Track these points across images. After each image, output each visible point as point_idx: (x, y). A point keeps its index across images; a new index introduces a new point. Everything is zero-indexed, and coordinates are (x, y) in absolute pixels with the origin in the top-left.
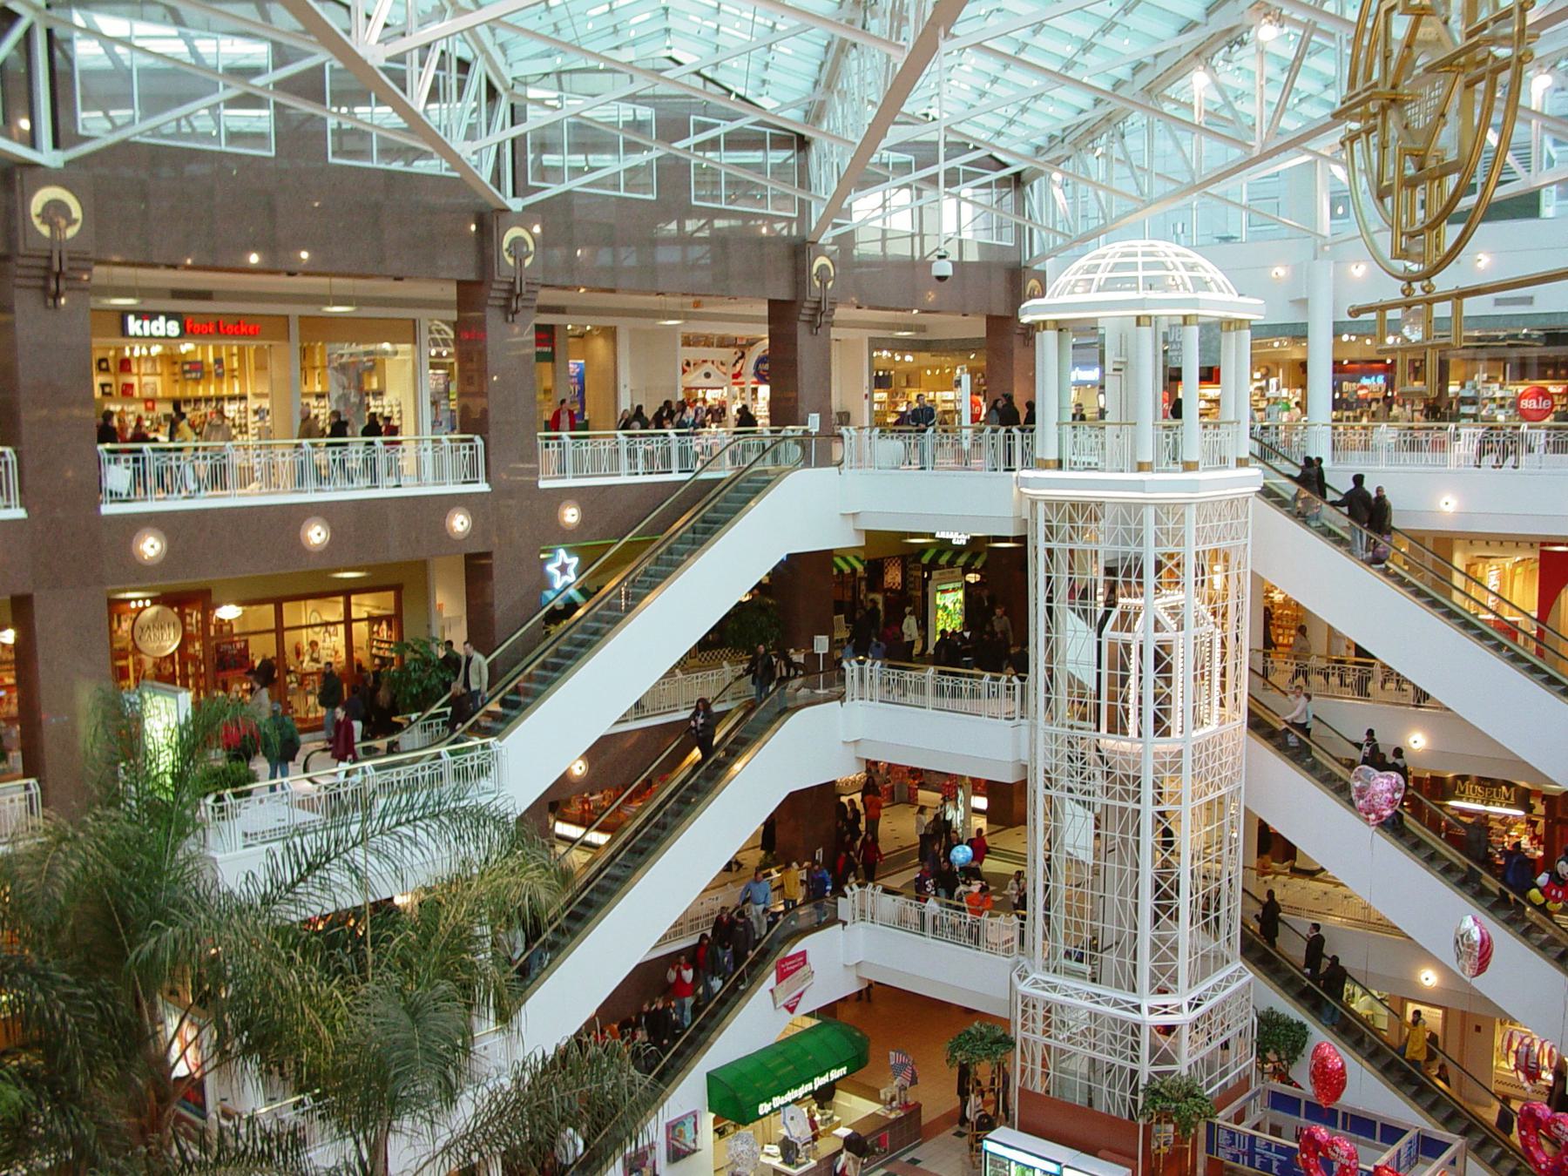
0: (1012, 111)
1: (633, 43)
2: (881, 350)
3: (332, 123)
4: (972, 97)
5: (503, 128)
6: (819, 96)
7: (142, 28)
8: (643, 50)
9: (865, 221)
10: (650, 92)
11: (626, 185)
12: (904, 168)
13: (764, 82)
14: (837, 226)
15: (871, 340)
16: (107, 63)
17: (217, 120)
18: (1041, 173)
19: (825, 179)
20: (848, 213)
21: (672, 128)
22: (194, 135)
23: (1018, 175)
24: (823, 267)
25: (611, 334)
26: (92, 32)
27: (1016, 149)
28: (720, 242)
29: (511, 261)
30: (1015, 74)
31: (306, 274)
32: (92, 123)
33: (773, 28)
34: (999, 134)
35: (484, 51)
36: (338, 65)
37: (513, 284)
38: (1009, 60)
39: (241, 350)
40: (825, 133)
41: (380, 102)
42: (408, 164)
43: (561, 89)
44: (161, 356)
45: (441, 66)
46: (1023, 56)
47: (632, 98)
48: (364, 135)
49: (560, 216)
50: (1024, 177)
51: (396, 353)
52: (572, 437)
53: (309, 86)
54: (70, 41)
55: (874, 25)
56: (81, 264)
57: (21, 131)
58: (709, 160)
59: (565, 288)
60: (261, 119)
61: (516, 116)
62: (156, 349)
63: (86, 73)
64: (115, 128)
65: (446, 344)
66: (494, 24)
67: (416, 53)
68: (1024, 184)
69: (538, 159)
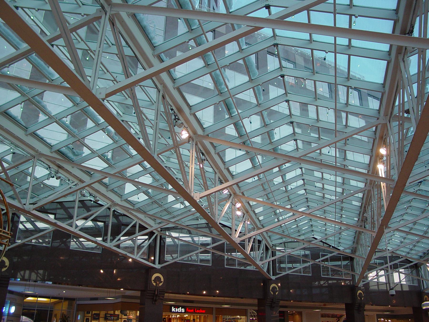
0: (411, 247)
1: (304, 234)
2: (381, 318)
3: (226, 257)
4: (398, 244)
5: (270, 258)
6: (355, 246)
7: (181, 235)
8: (307, 236)
9: (372, 279)
10: (308, 247)
11: (303, 272)
12: (381, 264)
13: (339, 243)
14: (363, 281)
15: (377, 315)
16: (172, 243)
17: (198, 256)
18: (422, 264)
19: (358, 270)
20: (367, 277)
21: (315, 255)
22: (191, 260)
23: (416, 264)
24: (360, 293)
25: (300, 314)
26: (170, 236)
27: (414, 256)
28: (330, 287)
29: (272, 293)
30: (410, 236)
31: (218, 296)
32: (168, 257)
33: (341, 228)
34: (408, 253)
35: (265, 238)
36: (228, 243)
37: (273, 299)
38: (408, 233)
39: (200, 316)
40: (358, 256)
41: (238, 252)
42: (245, 267)
43: (285, 247)
44: (179, 318)
45: (254, 242)
46: (412, 231)
47: (304, 249)
48: (234, 260)
49: (286, 281)
50: (418, 264)
51: (241, 319)
52: (269, 262)
53: (221, 248)
54: (165, 238)
55: (367, 226)
56: (162, 293)
57: (151, 260)
58: (326, 264)
59: (287, 301)
60: (208, 256)
61: (273, 254)
62: (178, 316)
63: (169, 246)
64: (173, 259)
65: (255, 317)
66: (267, 232)
67: (247, 239)
68: (418, 267)
69: (279, 266)
